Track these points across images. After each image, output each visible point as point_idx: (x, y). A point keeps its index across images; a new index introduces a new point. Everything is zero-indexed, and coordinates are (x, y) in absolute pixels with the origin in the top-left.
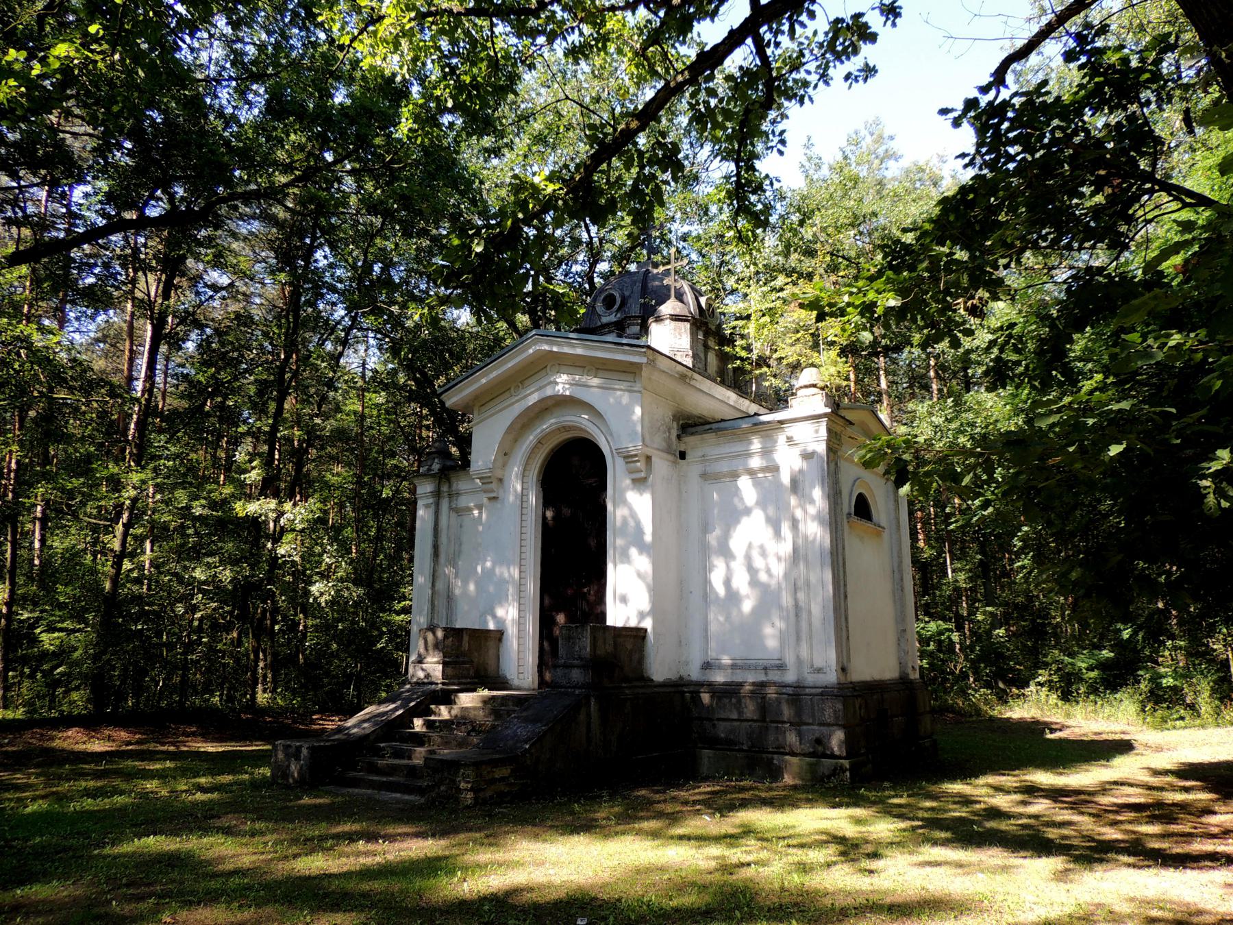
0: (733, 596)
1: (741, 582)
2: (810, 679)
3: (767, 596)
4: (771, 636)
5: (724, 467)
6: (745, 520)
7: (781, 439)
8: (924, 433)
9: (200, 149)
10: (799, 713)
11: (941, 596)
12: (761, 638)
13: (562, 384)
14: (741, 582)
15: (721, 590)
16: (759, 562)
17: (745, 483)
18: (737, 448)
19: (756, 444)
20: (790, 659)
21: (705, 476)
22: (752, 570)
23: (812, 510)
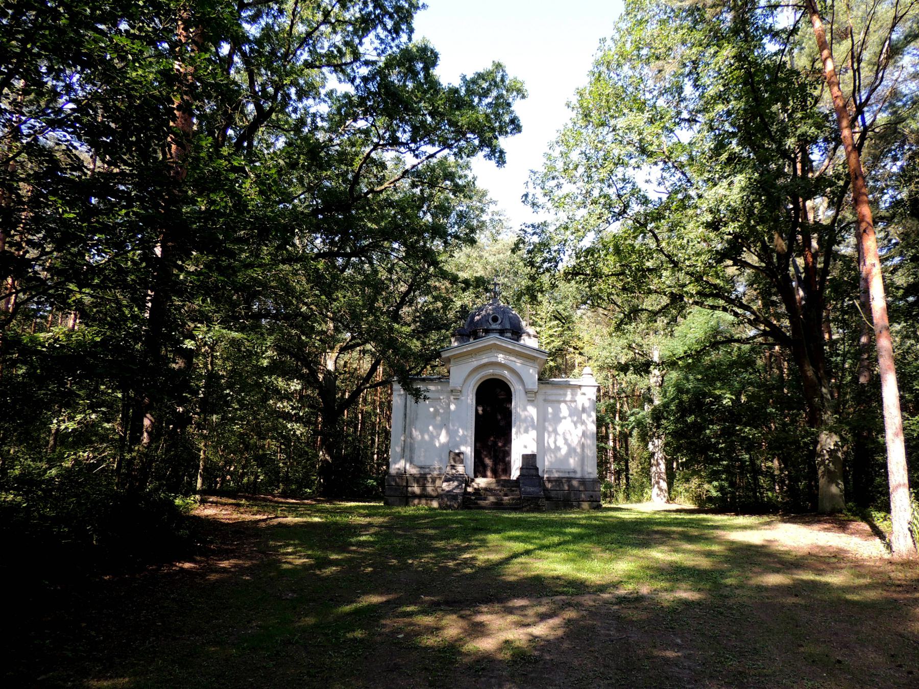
0: (558, 449)
1: (561, 443)
2: (587, 476)
3: (571, 451)
4: (572, 462)
5: (553, 398)
6: (563, 421)
7: (579, 392)
8: (592, 381)
9: (173, 45)
10: (585, 487)
11: (52, 279)
12: (569, 464)
13: (501, 358)
14: (561, 443)
15: (552, 446)
16: (568, 437)
17: (563, 406)
18: (561, 392)
19: (569, 392)
20: (579, 470)
21: (545, 400)
22: (566, 440)
23: (591, 419)
